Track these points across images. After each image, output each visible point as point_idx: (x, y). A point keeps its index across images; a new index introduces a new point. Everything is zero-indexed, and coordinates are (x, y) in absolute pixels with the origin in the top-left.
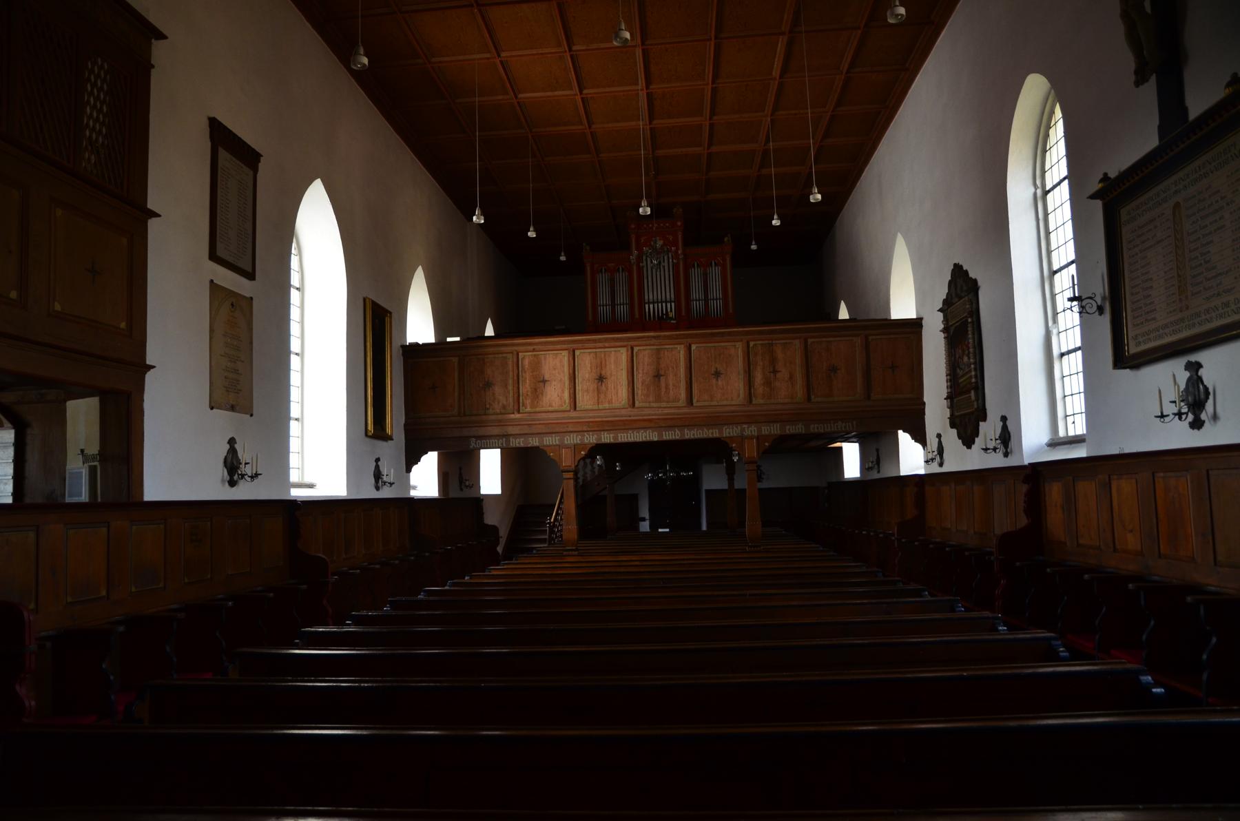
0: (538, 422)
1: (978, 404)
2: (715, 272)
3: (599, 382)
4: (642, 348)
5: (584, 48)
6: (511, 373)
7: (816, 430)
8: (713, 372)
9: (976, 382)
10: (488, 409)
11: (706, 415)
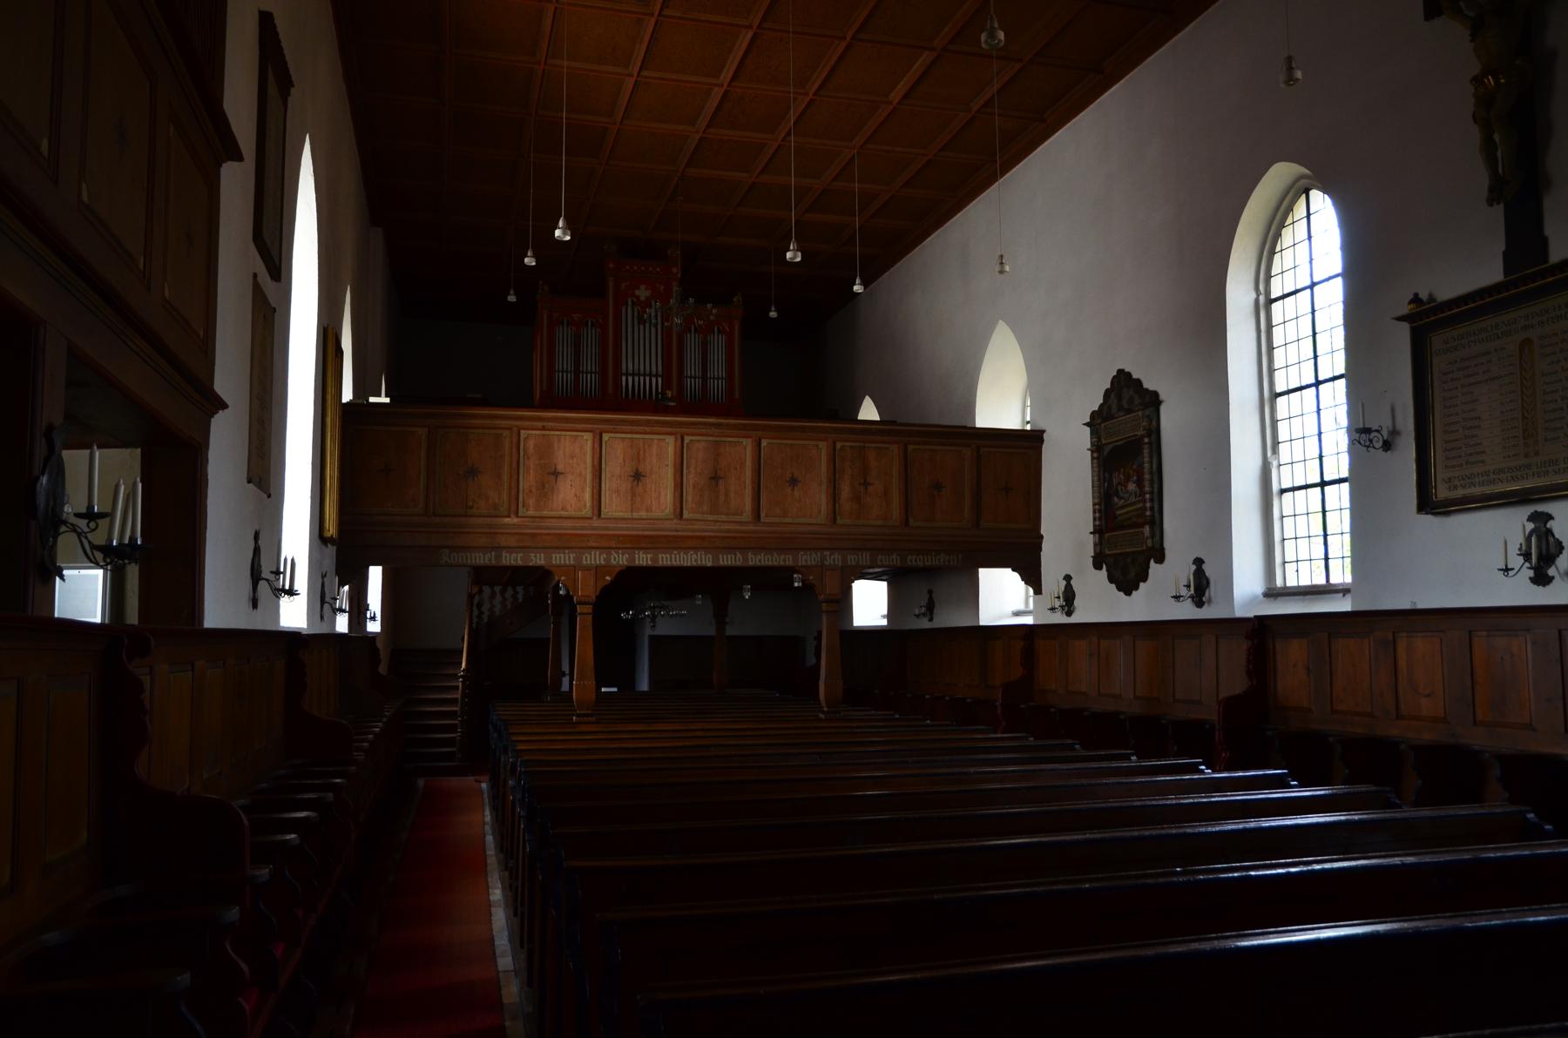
0: (546, 532)
2: (718, 343)
5: (679, 15)
6: (507, 458)
7: (914, 563)
10: (472, 507)
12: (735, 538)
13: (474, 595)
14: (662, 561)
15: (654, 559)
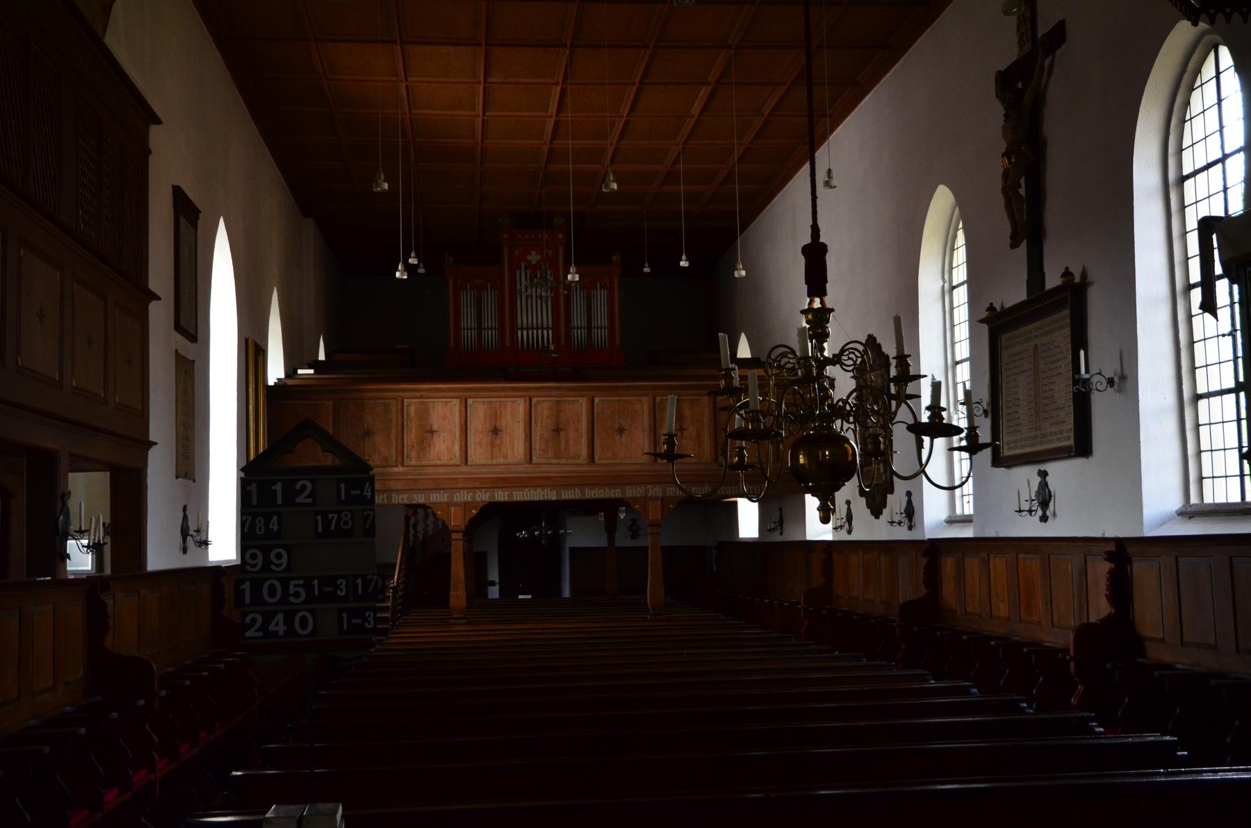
0: (424, 477)
3: (493, 434)
4: (541, 399)
5: (500, 81)
6: (394, 422)
12: (573, 477)
13: (410, 517)
14: (517, 497)
15: (510, 495)
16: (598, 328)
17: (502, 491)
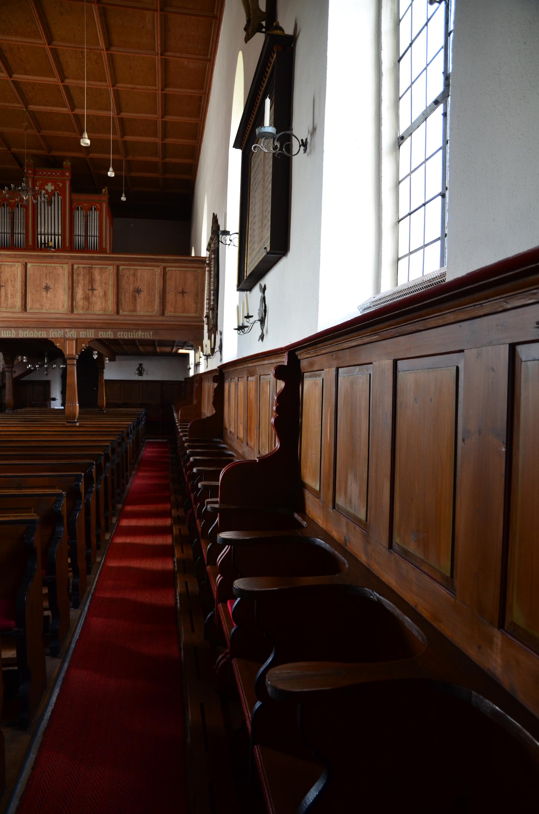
1: (213, 321)
2: (94, 215)
7: (122, 337)
8: (44, 287)
9: (213, 305)
11: (37, 320)
16: (92, 236)
17: (38, 331)
